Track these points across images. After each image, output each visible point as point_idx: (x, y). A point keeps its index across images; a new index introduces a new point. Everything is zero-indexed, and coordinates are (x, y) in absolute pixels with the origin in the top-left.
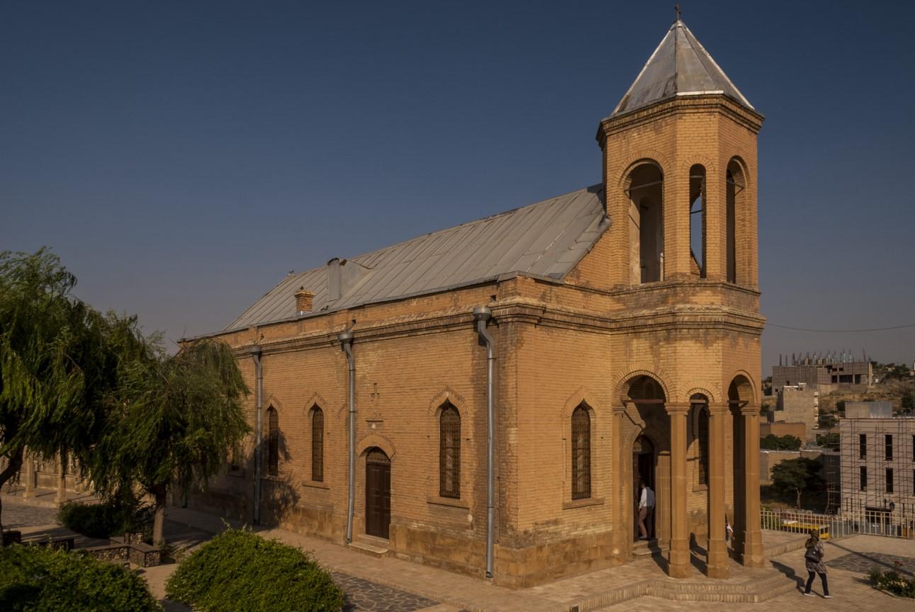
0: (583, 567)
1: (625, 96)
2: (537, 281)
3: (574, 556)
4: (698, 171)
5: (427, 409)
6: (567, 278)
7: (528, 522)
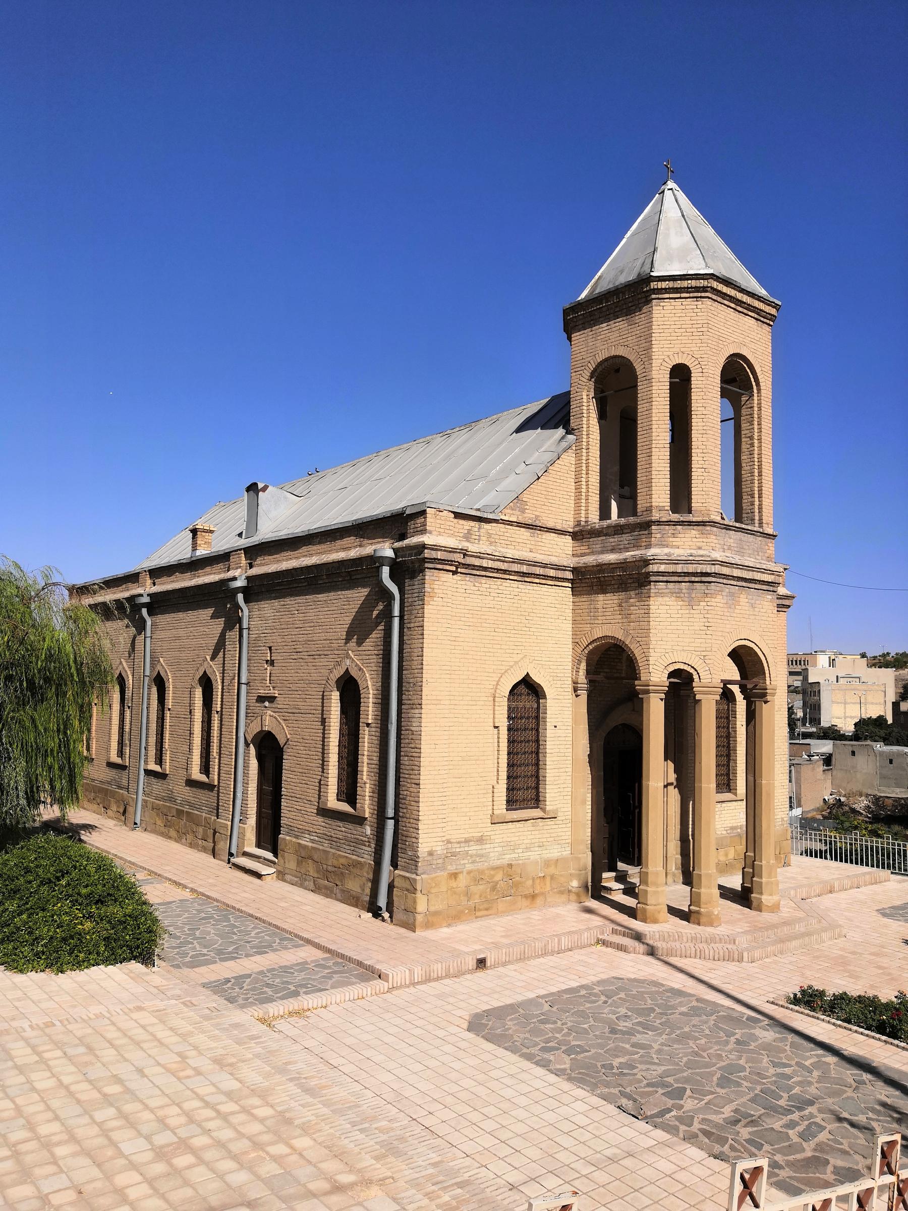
0: (525, 903)
1: (597, 277)
2: (458, 515)
3: (510, 887)
4: (681, 377)
5: (324, 682)
6: (506, 511)
7: (435, 839)
